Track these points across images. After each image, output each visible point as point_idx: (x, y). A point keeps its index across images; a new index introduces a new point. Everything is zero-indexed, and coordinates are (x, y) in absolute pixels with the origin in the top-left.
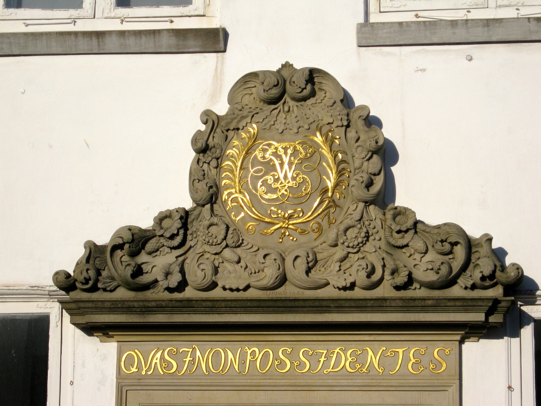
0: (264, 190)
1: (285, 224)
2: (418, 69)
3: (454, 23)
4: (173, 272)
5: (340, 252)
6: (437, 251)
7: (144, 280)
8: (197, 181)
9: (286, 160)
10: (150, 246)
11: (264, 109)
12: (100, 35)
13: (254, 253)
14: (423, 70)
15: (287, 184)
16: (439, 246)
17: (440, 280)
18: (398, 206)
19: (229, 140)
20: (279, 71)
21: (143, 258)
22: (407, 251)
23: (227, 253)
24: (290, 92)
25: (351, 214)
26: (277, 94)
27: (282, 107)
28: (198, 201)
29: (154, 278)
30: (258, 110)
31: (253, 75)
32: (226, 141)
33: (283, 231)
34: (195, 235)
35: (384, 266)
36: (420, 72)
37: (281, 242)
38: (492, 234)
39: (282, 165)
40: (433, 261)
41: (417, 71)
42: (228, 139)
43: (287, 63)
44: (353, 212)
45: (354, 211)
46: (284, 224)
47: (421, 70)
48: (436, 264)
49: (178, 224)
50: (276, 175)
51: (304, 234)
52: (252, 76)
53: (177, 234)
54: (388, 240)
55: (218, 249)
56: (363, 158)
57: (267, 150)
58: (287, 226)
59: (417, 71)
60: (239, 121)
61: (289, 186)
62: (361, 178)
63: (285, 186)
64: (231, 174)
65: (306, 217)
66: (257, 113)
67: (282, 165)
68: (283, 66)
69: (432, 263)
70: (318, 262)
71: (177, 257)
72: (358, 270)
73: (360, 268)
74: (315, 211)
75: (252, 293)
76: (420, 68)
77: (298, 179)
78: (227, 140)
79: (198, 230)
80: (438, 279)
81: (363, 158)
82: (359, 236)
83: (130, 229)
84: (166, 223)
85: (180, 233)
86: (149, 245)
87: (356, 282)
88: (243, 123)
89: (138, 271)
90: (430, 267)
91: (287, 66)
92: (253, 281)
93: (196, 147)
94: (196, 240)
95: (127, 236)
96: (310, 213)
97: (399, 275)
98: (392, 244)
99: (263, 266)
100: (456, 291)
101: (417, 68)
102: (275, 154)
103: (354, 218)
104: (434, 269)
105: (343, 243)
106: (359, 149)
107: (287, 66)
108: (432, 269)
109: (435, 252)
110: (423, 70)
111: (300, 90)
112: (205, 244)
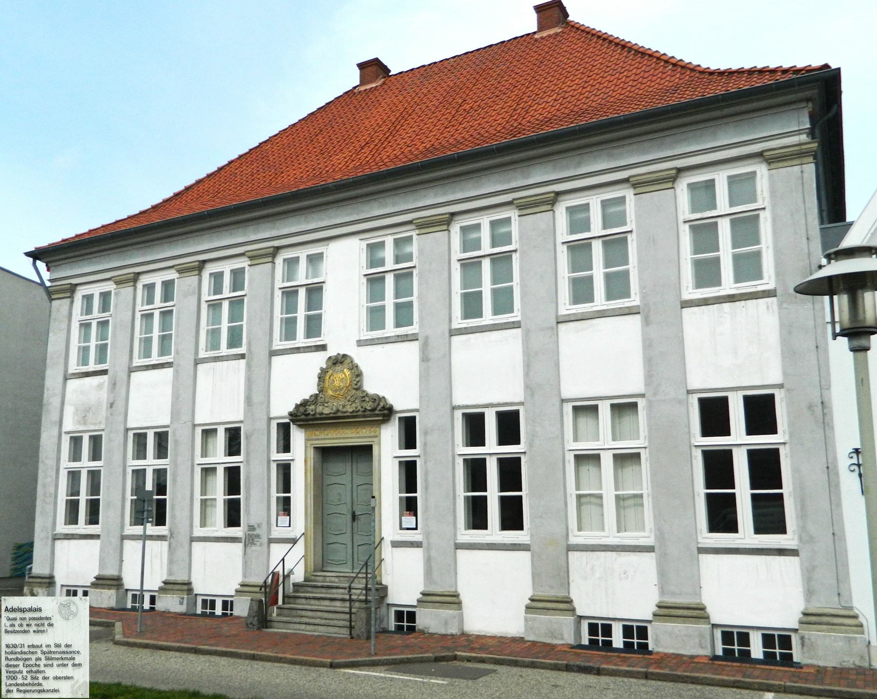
3: (378, 339)
5: (350, 403)
10: (309, 403)
12: (298, 348)
21: (307, 407)
23: (326, 405)
75: (332, 415)
89: (306, 411)
95: (303, 401)
100: (377, 412)
107: (339, 354)
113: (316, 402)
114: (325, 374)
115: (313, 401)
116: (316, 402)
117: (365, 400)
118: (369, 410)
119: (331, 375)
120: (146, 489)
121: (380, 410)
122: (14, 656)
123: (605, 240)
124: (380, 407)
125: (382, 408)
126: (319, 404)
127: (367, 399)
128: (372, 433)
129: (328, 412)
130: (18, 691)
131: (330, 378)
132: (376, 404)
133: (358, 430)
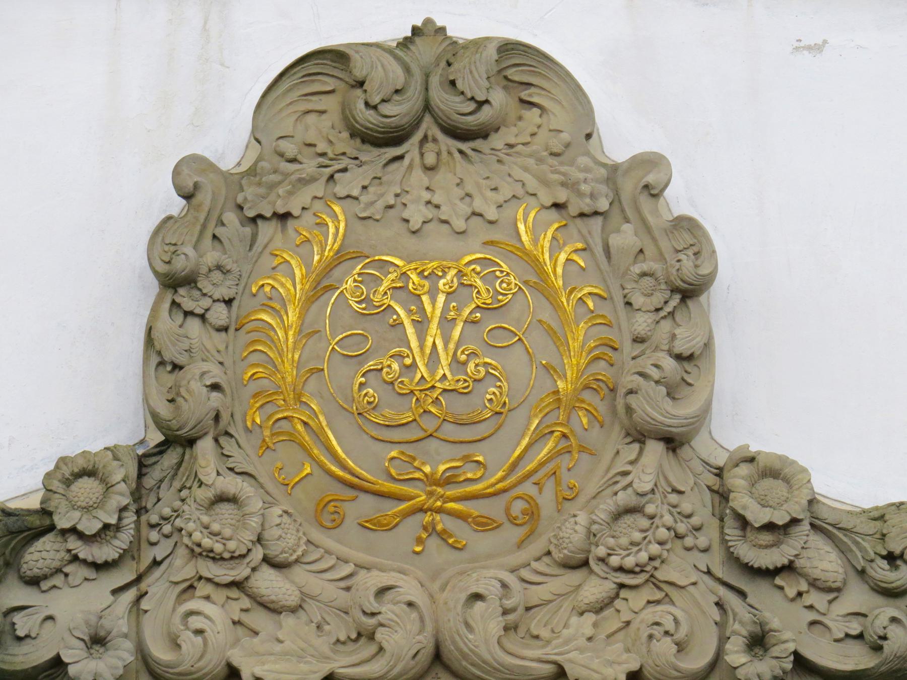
0: (372, 399)
1: (431, 501)
2: (802, 44)
4: (108, 638)
6: (876, 584)
7: (20, 659)
8: (169, 368)
9: (435, 308)
11: (363, 158)
13: (343, 584)
14: (817, 48)
15: (438, 385)
17: (883, 668)
18: (759, 453)
19: (260, 250)
22: (787, 583)
24: (442, 111)
25: (625, 474)
26: (405, 116)
27: (415, 153)
28: (175, 428)
29: (48, 655)
30: (344, 162)
31: (329, 56)
32: (250, 250)
33: (427, 519)
34: (167, 529)
36: (806, 53)
37: (417, 553)
39: (421, 325)
40: (863, 611)
41: (797, 49)
42: (257, 245)
43: (428, 22)
44: (629, 468)
45: (632, 463)
46: (430, 498)
47: (809, 48)
48: (872, 624)
50: (408, 356)
51: (490, 530)
52: (327, 59)
53: (118, 528)
54: (732, 550)
56: (658, 310)
57: (378, 281)
58: (439, 503)
59: (797, 49)
61: (445, 390)
62: (655, 369)
63: (433, 387)
64: (271, 348)
65: (493, 480)
66: (344, 170)
67: (421, 325)
68: (416, 31)
69: (861, 619)
70: (794, 515)
71: (116, 592)
72: (651, 637)
73: (657, 631)
74: (407, 482)
76: (807, 43)
77: (471, 366)
78: (255, 248)
79: (176, 514)
80: (878, 666)
81: (658, 310)
82: (650, 537)
85: (125, 522)
86: (36, 556)
87: (643, 669)
88: (304, 197)
90: (855, 629)
93: (162, 268)
94: (170, 543)
96: (500, 474)
97: (766, 650)
98: (746, 561)
99: (372, 621)
101: (800, 41)
102: (400, 290)
103: (635, 485)
104: (866, 636)
106: (647, 281)
108: (860, 636)
109: (867, 586)
110: (817, 48)
111: (472, 106)
112: (200, 554)
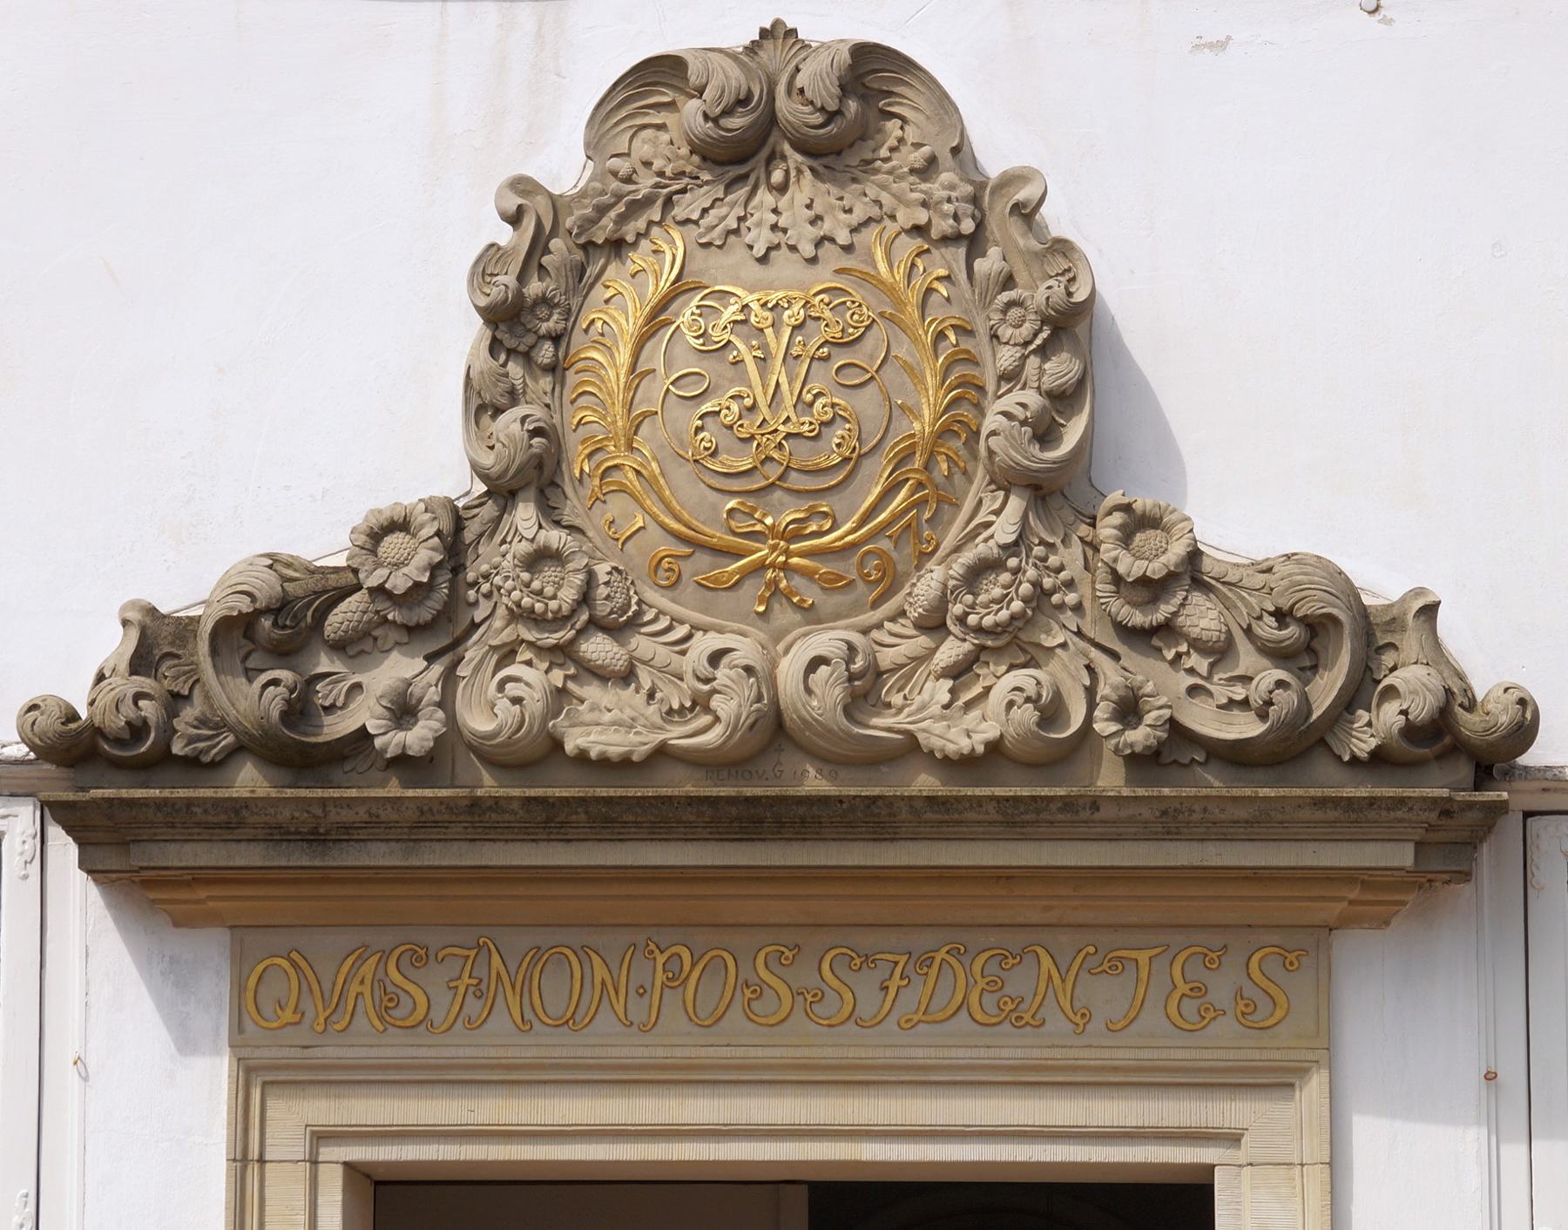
5: (951, 650)
16: (1268, 629)
20: (752, 49)
23: (598, 648)
35: (1091, 692)
38: (1439, 590)
49: (427, 554)
55: (565, 635)
60: (622, 219)
68: (764, 33)
75: (687, 785)
83: (275, 561)
84: (394, 545)
89: (300, 710)
91: (776, 34)
92: (677, 735)
95: (266, 586)
105: (961, 620)
113: (446, 614)
114: (580, 278)
115: (418, 590)
116: (446, 614)
117: (1167, 629)
118: (1233, 756)
119: (680, 289)
120: (486, 489)
121: (1380, 759)
122: (530, 830)
123: (985, 188)
124: (1389, 716)
125: (1411, 732)
126: (499, 631)
127: (1202, 617)
128: (1225, 1027)
129: (639, 742)
130: (474, 827)
131: (657, 319)
132: (1326, 688)
133: (1019, 982)
